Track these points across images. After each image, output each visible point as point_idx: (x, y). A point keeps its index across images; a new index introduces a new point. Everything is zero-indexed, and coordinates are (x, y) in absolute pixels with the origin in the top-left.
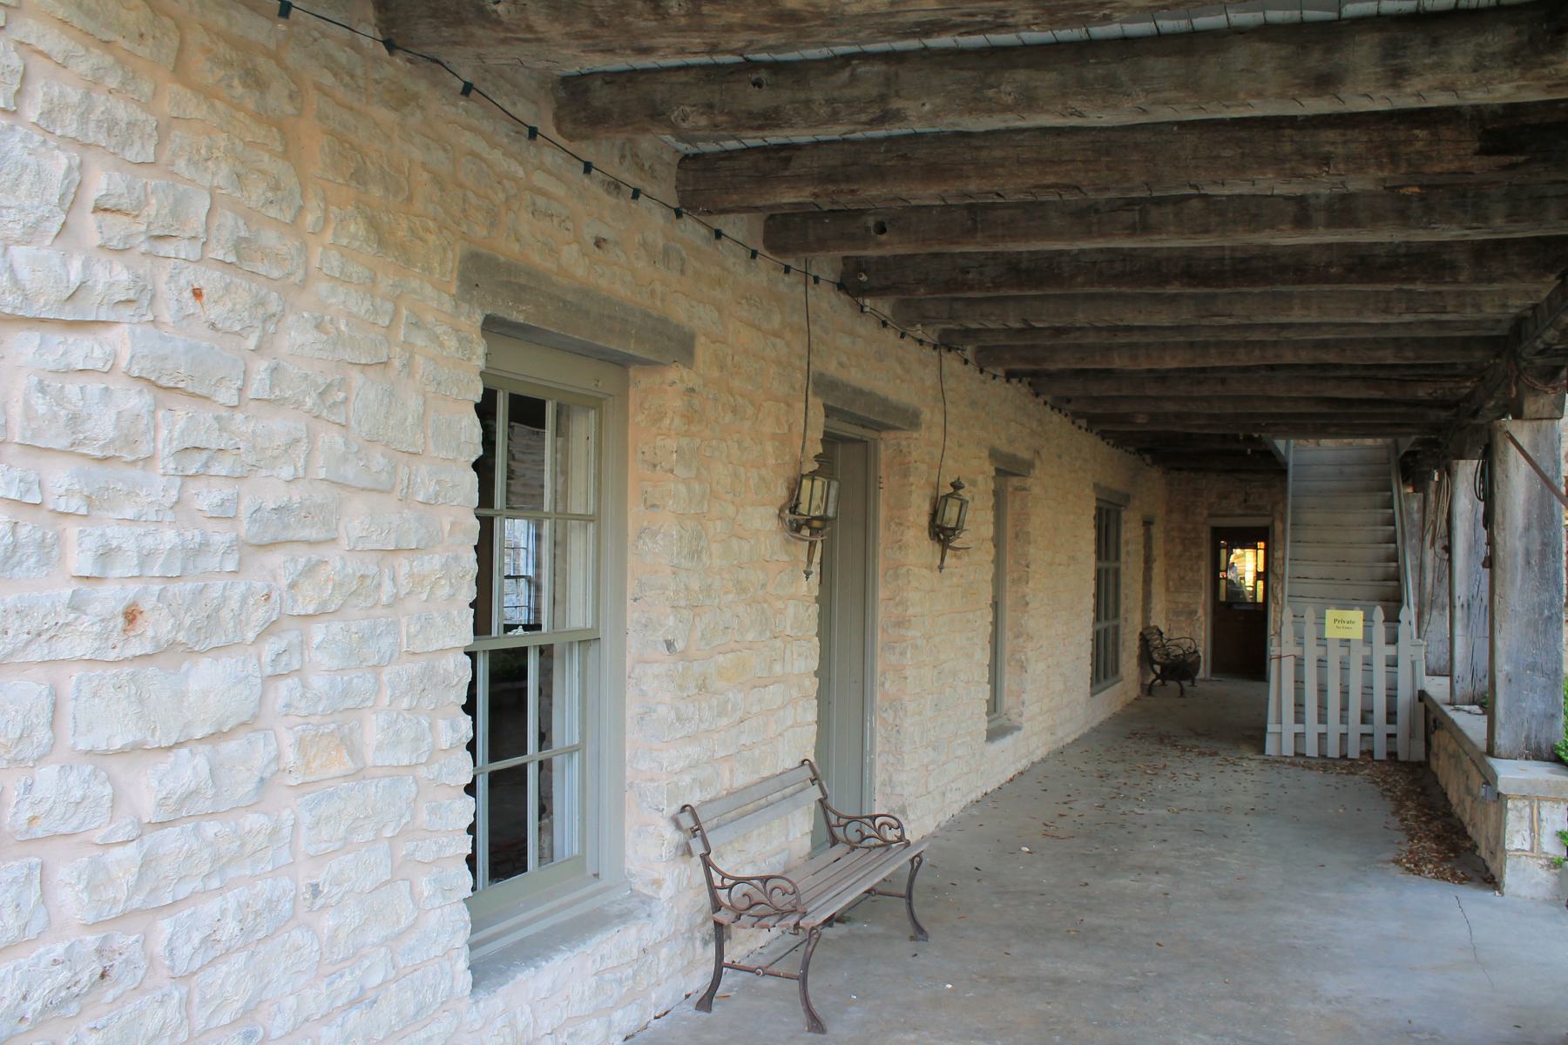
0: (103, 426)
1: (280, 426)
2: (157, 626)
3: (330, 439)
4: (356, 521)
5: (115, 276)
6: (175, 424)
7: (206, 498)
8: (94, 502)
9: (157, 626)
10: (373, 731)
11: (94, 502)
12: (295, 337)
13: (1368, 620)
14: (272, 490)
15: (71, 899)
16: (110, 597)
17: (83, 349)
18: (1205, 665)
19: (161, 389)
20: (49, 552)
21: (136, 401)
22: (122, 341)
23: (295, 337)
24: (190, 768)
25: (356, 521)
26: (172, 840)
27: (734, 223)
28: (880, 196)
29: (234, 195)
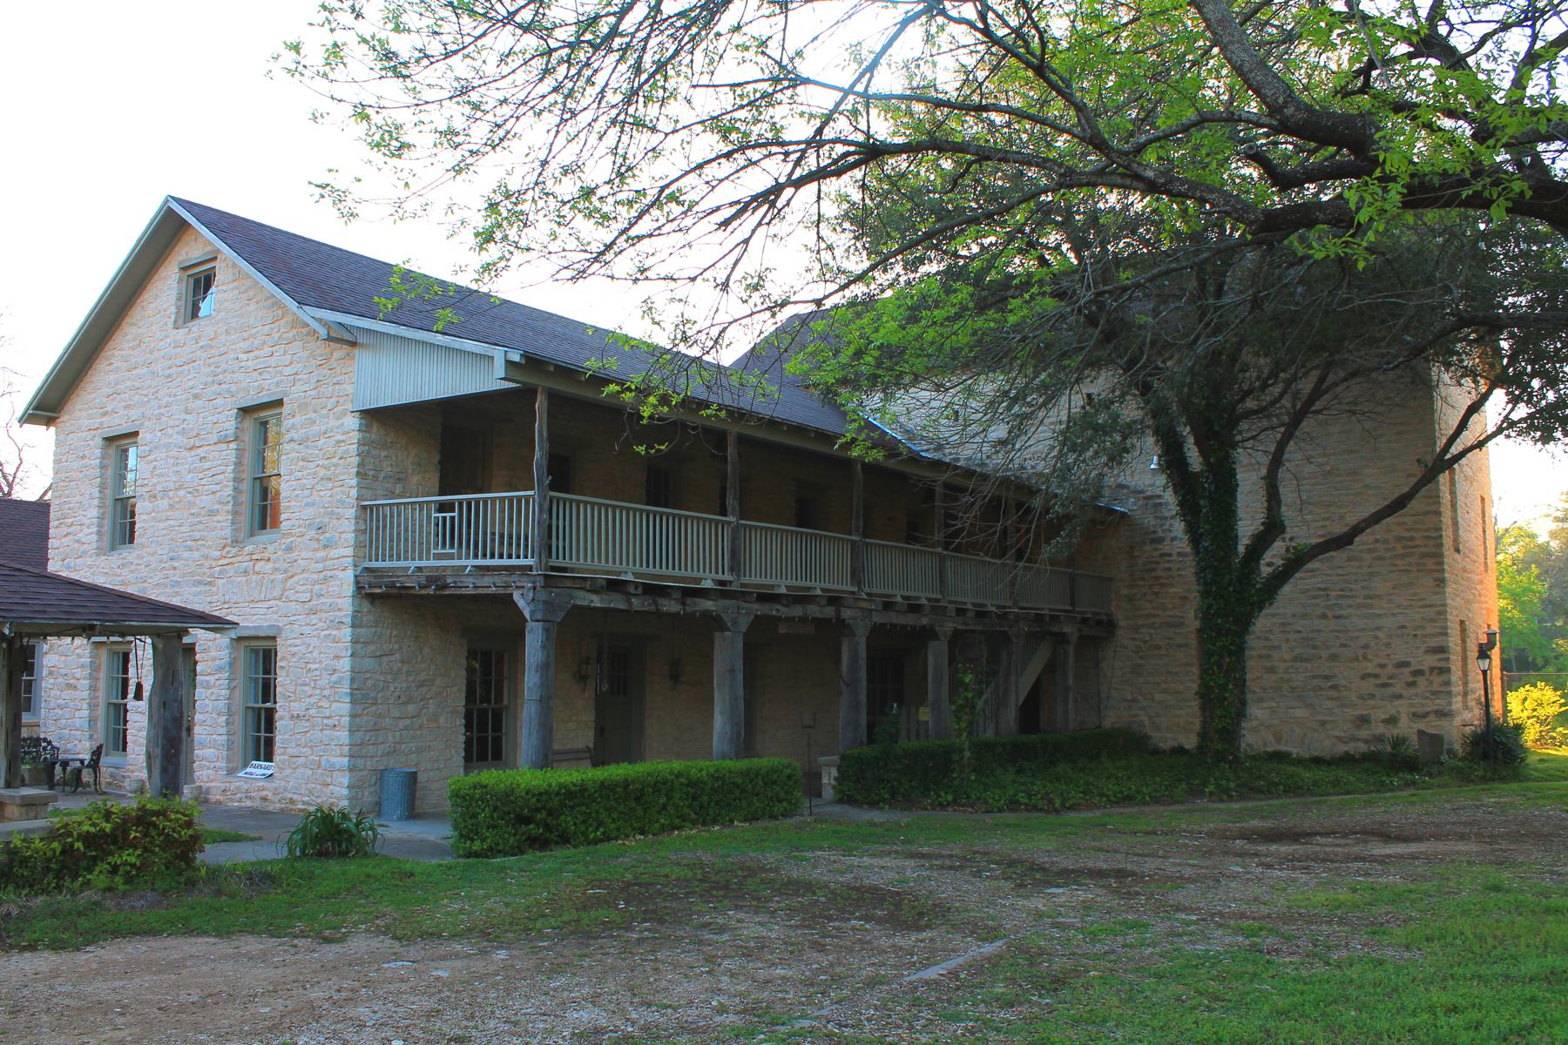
0: (395, 669)
1: (423, 666)
2: (403, 699)
3: (433, 667)
4: (438, 681)
5: (397, 646)
6: (405, 668)
7: (411, 679)
8: (394, 680)
9: (403, 699)
10: (442, 720)
11: (394, 680)
12: (426, 650)
13: (1506, 711)
14: (423, 676)
15: (390, 738)
16: (396, 694)
17: (392, 658)
18: (540, 420)
19: (403, 662)
20: (388, 687)
21: (400, 665)
22: (397, 656)
23: (426, 650)
24: (408, 722)
25: (438, 681)
26: (405, 733)
27: (899, 307)
28: (918, 970)
29: (1379, 169)
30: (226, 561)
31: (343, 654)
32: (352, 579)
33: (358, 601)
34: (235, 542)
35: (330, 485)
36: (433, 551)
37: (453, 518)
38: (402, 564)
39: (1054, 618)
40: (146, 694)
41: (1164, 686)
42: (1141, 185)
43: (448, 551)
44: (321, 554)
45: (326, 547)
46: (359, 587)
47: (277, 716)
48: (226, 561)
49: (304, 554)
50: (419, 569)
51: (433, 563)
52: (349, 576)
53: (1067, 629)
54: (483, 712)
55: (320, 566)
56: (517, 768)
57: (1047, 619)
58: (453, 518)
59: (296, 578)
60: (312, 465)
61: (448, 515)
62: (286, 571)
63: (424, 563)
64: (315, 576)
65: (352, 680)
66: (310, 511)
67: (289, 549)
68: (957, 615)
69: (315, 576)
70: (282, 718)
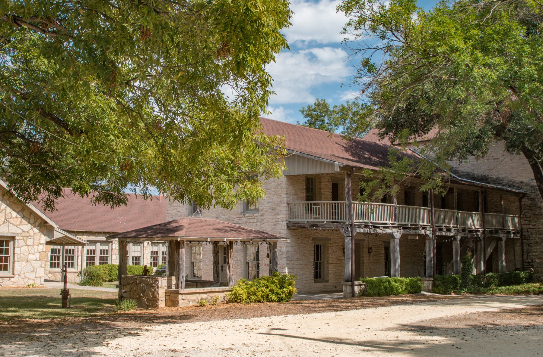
30: (238, 219)
31: (284, 246)
32: (286, 224)
33: (287, 231)
34: (243, 212)
35: (276, 197)
36: (312, 217)
37: (319, 208)
38: (302, 220)
39: (497, 232)
40: (366, 250)
41: (539, 256)
42: (499, 243)
43: (318, 217)
44: (273, 217)
45: (275, 215)
46: (288, 227)
47: (260, 265)
48: (238, 219)
49: (268, 217)
50: (308, 222)
51: (312, 220)
52: (285, 223)
53: (501, 235)
54: (317, 263)
55: (274, 220)
56: (315, 282)
57: (494, 232)
58: (319, 208)
59: (265, 224)
60: (269, 191)
61: (317, 207)
62: (261, 222)
63: (310, 220)
64: (272, 223)
65: (287, 254)
66: (270, 205)
67: (262, 215)
68: (462, 232)
69: (272, 223)
70: (261, 265)
